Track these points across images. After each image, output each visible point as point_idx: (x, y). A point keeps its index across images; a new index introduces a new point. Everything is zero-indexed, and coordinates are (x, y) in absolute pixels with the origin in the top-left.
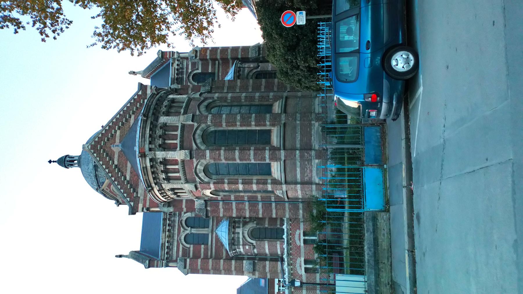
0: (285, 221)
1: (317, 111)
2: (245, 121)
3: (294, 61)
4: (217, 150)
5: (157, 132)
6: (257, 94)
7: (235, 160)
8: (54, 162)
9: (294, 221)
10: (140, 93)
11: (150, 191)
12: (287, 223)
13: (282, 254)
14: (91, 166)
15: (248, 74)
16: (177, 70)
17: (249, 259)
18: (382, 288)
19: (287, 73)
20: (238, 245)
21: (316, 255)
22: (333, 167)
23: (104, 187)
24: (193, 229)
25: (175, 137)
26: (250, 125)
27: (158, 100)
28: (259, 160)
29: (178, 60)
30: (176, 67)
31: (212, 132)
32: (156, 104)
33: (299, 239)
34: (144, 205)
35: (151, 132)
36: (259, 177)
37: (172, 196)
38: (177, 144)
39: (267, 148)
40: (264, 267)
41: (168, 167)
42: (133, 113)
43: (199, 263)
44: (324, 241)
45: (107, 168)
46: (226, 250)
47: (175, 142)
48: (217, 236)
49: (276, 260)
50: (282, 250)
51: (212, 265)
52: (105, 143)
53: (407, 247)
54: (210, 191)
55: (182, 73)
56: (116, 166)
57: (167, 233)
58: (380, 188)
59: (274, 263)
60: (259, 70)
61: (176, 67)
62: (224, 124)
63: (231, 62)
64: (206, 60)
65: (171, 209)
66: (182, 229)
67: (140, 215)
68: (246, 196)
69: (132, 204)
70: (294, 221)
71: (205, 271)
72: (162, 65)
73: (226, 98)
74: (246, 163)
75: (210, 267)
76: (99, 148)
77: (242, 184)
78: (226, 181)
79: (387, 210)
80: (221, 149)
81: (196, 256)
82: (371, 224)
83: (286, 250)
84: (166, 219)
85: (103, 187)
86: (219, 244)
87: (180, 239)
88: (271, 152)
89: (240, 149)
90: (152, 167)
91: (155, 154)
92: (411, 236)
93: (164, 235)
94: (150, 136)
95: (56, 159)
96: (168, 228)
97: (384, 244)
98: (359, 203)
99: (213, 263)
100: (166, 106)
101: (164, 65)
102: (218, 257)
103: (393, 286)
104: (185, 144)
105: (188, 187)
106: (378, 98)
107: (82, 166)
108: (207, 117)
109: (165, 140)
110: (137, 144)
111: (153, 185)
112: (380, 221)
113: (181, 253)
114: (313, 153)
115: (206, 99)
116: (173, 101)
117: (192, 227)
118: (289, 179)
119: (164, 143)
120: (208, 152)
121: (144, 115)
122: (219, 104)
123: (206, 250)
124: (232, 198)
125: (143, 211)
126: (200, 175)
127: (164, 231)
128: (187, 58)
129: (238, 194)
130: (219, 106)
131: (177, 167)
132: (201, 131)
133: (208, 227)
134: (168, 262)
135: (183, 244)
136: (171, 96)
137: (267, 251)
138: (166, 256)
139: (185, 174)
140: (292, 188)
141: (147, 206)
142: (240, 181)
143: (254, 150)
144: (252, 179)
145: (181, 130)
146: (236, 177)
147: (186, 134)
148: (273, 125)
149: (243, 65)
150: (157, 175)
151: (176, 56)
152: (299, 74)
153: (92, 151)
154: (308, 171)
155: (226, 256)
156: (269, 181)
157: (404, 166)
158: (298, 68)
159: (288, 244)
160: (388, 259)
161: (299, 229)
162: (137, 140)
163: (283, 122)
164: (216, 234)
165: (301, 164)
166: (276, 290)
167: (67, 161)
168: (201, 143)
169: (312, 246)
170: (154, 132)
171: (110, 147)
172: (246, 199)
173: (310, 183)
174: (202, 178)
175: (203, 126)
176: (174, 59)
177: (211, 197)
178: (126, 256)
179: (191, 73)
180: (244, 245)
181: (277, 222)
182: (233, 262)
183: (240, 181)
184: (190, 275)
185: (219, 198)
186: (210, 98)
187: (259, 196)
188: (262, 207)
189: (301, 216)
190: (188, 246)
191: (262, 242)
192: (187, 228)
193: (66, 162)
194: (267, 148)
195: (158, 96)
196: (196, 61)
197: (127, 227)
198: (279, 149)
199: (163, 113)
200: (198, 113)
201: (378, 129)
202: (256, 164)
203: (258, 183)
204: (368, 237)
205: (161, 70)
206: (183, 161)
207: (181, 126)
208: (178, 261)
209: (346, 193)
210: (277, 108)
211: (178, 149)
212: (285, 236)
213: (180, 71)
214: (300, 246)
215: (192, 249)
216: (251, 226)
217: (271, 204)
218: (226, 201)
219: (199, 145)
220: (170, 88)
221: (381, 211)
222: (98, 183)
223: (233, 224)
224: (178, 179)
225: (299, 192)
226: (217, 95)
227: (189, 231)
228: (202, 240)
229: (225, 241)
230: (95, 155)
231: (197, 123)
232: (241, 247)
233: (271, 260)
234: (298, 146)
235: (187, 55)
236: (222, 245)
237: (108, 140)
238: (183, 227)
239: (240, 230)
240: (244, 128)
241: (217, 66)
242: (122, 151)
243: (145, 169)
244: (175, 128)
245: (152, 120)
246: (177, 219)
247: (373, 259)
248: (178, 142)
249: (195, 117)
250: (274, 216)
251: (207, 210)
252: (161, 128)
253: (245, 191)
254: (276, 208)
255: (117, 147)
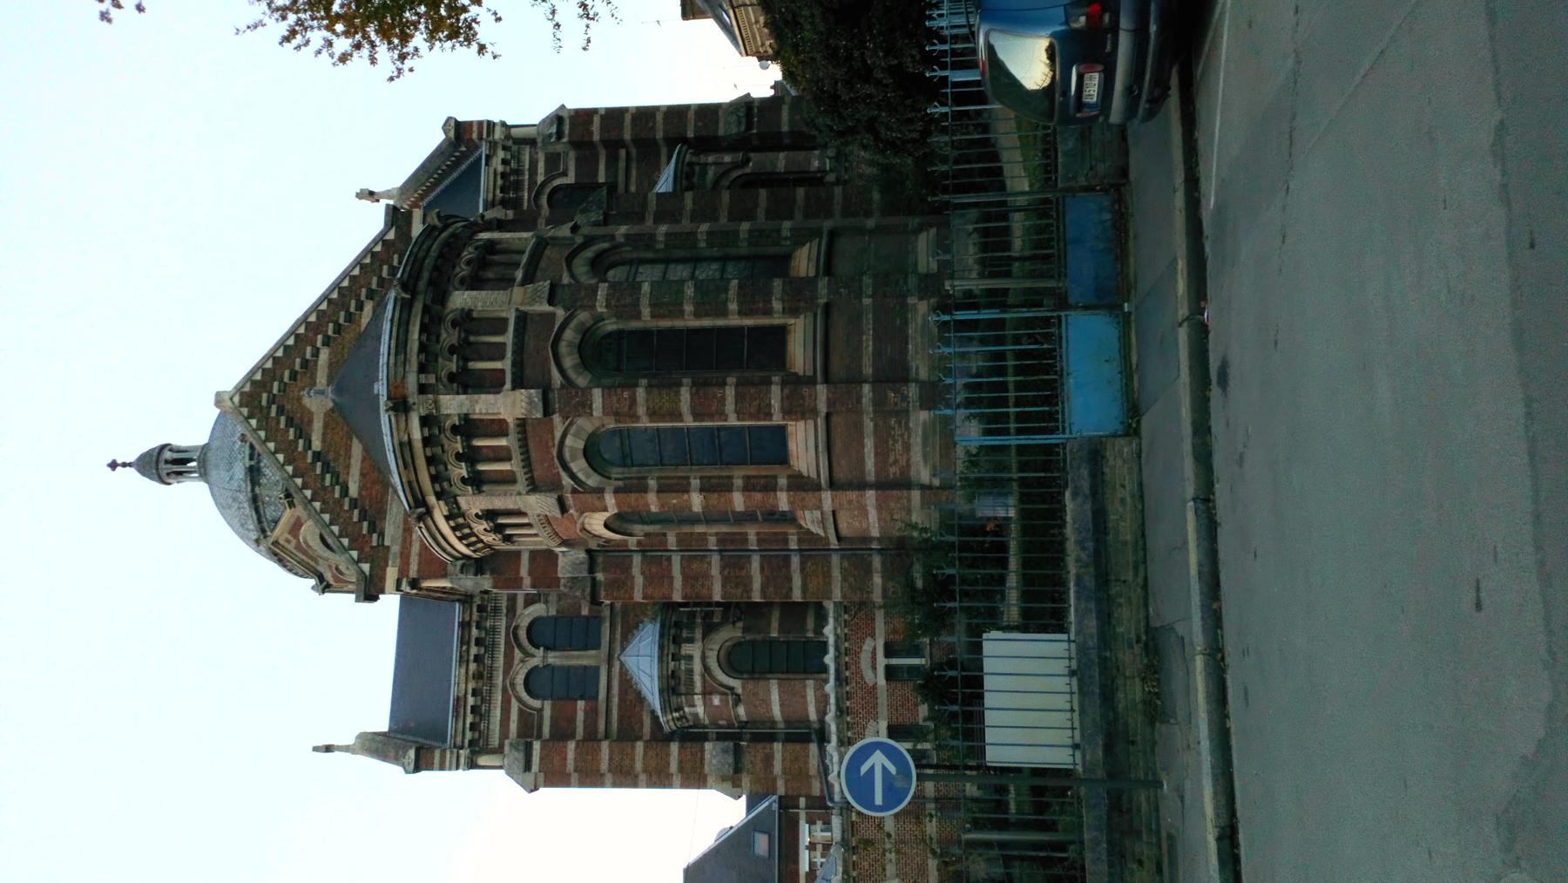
0: (831, 614)
1: (922, 269)
2: (710, 300)
3: (856, 54)
4: (623, 386)
5: (444, 335)
6: (745, 226)
7: (678, 416)
8: (124, 465)
9: (857, 611)
10: (391, 235)
11: (420, 518)
12: (836, 620)
13: (822, 713)
14: (239, 471)
15: (716, 183)
16: (503, 175)
17: (720, 737)
18: (1120, 656)
19: (835, 97)
20: (690, 693)
21: (923, 710)
22: (971, 435)
23: (280, 532)
24: (551, 654)
25: (497, 352)
26: (723, 313)
27: (447, 244)
28: (752, 417)
29: (504, 148)
30: (500, 168)
31: (610, 334)
32: (441, 255)
33: (873, 664)
34: (403, 572)
35: (424, 338)
36: (752, 471)
37: (489, 538)
38: (502, 371)
39: (776, 379)
40: (768, 760)
41: (478, 443)
42: (370, 296)
43: (571, 755)
44: (952, 664)
45: (288, 461)
46: (653, 712)
47: (498, 365)
48: (624, 672)
49: (804, 739)
50: (823, 701)
51: (611, 759)
52: (284, 388)
53: (1190, 491)
54: (606, 515)
55: (518, 186)
56: (317, 456)
57: (473, 666)
58: (1111, 371)
59: (798, 746)
60: (748, 170)
61: (500, 168)
62: (646, 312)
63: (664, 151)
64: (591, 145)
65: (486, 582)
66: (518, 654)
67: (390, 603)
68: (712, 533)
69: (366, 567)
70: (857, 611)
71: (590, 777)
72: (456, 164)
73: (652, 236)
74: (711, 428)
75: (604, 766)
76: (264, 403)
77: (702, 490)
78: (652, 483)
79: (1131, 430)
80: (637, 385)
81: (562, 732)
82: (1085, 472)
83: (832, 700)
84: (469, 624)
85: (277, 531)
86: (631, 697)
87: (513, 685)
88: (787, 391)
89: (694, 384)
90: (426, 442)
91: (436, 402)
92: (1204, 457)
93: (463, 671)
94: (423, 348)
95: (132, 458)
96: (474, 650)
97: (1122, 525)
98: (1051, 416)
99: (611, 753)
100: (468, 263)
101: (464, 167)
102: (627, 734)
103: (1151, 644)
104: (528, 372)
105: (539, 505)
106: (1107, 18)
107: (213, 474)
108: (594, 290)
109: (466, 360)
110: (382, 374)
111: (432, 499)
112: (1111, 463)
113: (513, 726)
114: (913, 391)
115: (589, 241)
116: (491, 246)
117: (547, 649)
118: (840, 475)
119: (464, 370)
120: (597, 393)
121: (404, 286)
122: (628, 256)
123: (592, 714)
124: (672, 540)
125: (398, 589)
126: (574, 467)
127: (463, 660)
128: (531, 142)
129: (687, 529)
130: (630, 262)
131: (503, 442)
132: (576, 330)
133: (597, 646)
134: (476, 752)
135: (519, 700)
136: (485, 236)
137: (777, 712)
138: (469, 735)
139: (527, 462)
140: (850, 502)
141: (413, 573)
142: (695, 483)
143: (737, 385)
144: (730, 477)
145: (516, 330)
146: (682, 472)
147: (530, 343)
148: (793, 311)
149: (702, 159)
150: (441, 467)
151: (498, 134)
152: (870, 96)
153: (245, 411)
154: (899, 446)
155: (652, 732)
156: (783, 481)
157: (1181, 264)
158: (866, 75)
159: (840, 680)
160: (1136, 568)
161: (873, 636)
162: (383, 360)
163: (822, 301)
164: (622, 665)
165: (876, 426)
166: (804, 867)
167: (167, 462)
168: (575, 367)
169: (911, 684)
170: (433, 338)
171: (299, 399)
172: (712, 543)
173: (904, 483)
174: (581, 476)
175: (583, 316)
176: (493, 145)
177: (608, 541)
178: (346, 749)
179: (543, 184)
180: (706, 693)
181: (804, 624)
182: (674, 747)
183: (695, 483)
184: (542, 790)
185: (632, 542)
186: (603, 238)
187: (752, 532)
188: (762, 568)
189: (877, 597)
190: (536, 703)
191: (762, 683)
192: (532, 650)
193: (164, 464)
194: (776, 379)
195: (444, 235)
196: (559, 148)
197: (355, 647)
198: (811, 381)
199: (462, 282)
200: (566, 280)
201: (1106, 201)
202: (743, 428)
203: (749, 487)
204: (1073, 508)
205: (447, 188)
206: (522, 424)
207: (517, 318)
208: (507, 748)
209: (1012, 501)
210: (804, 262)
211: (508, 385)
212: (829, 659)
213: (510, 182)
214: (875, 687)
215: (547, 713)
216: (729, 634)
217: (787, 560)
218: (653, 552)
219: (572, 374)
220: (482, 216)
221: (1115, 436)
222: (260, 521)
223: (673, 631)
224: (508, 479)
225: (873, 515)
226: (623, 229)
227: (538, 658)
228: (581, 684)
229: (648, 680)
230: (254, 422)
231: (566, 309)
232: (698, 699)
233: (789, 739)
234: (868, 370)
235: (533, 131)
236: (640, 698)
237: (294, 376)
238: (520, 646)
239: (694, 650)
240: (707, 323)
241: (622, 164)
242: (337, 408)
243: (405, 447)
244: (498, 325)
245: (429, 302)
246: (502, 624)
247: (1092, 570)
248: (505, 365)
249: (559, 291)
250: (797, 596)
251: (594, 579)
252: (454, 324)
253: (708, 518)
254: (803, 570)
255: (320, 397)
